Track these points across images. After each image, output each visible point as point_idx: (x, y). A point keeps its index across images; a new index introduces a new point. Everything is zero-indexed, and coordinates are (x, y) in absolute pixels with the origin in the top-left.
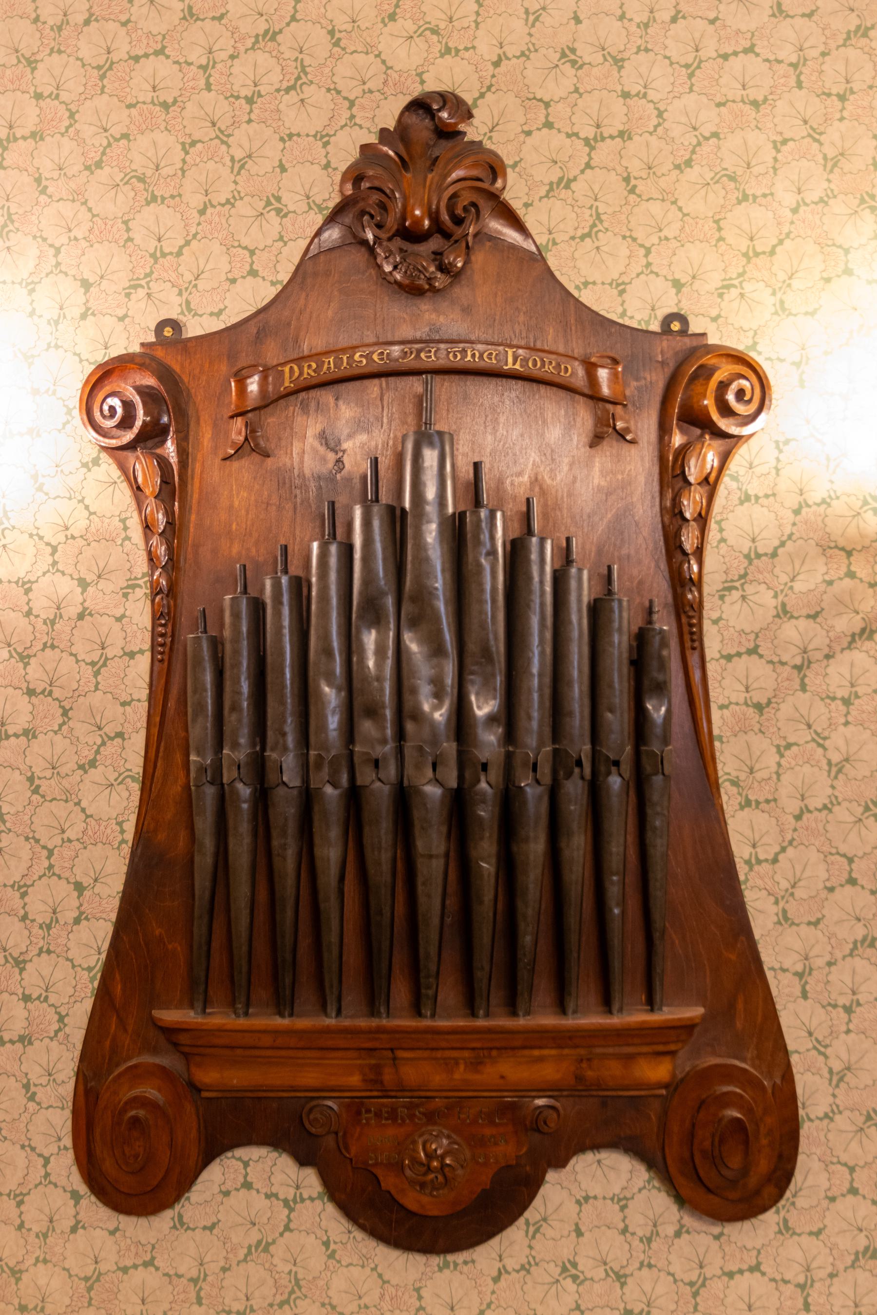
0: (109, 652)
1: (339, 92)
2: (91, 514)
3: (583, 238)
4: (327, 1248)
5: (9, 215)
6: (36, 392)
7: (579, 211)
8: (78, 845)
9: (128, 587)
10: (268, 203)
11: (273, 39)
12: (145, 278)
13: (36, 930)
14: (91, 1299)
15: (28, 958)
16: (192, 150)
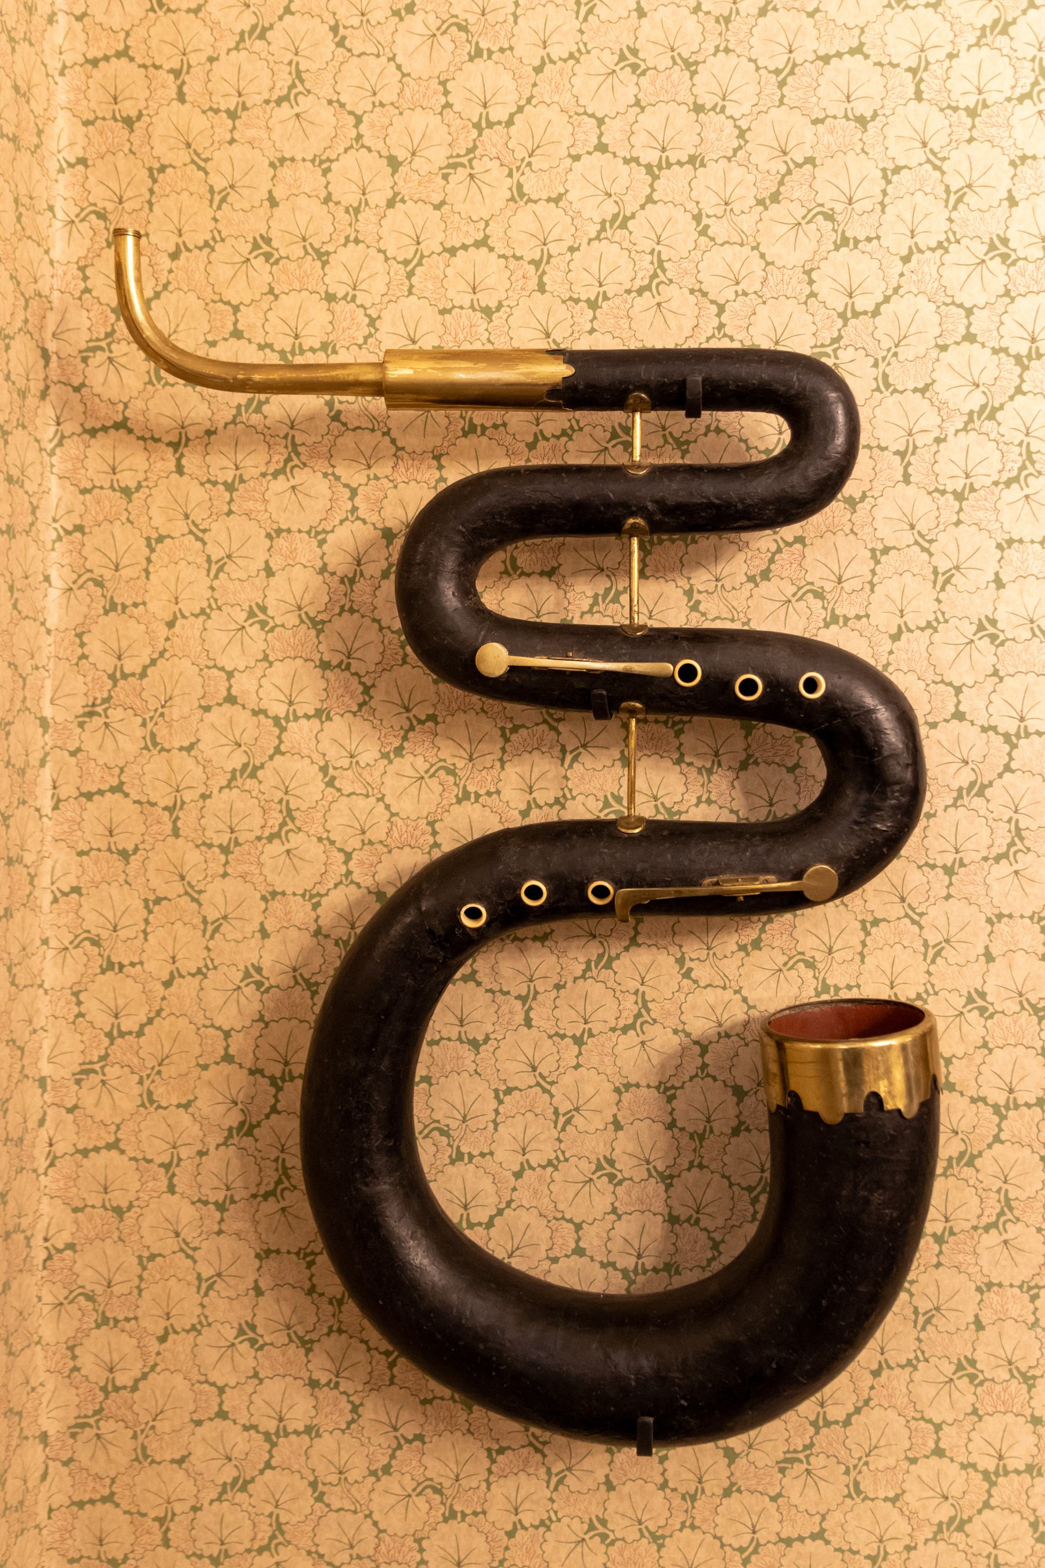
1: (705, 294)
3: (640, 291)
4: (682, 966)
5: (294, 445)
6: (325, 665)
7: (1005, 448)
9: (449, 166)
10: (592, 1527)
14: (411, 286)
15: (701, 58)
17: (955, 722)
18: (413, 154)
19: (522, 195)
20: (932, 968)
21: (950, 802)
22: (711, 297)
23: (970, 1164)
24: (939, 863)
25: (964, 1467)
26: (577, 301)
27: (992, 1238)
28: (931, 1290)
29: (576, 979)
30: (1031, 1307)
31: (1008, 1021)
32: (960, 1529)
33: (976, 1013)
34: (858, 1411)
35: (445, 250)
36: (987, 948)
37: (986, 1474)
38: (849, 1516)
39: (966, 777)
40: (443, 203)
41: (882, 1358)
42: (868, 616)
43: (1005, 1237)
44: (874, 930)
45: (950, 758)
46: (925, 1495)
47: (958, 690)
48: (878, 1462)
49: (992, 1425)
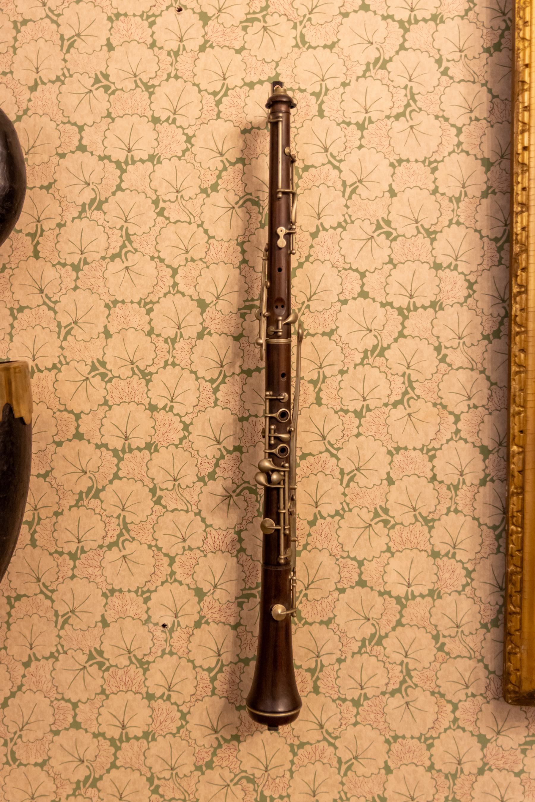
0: (230, 82)
2: (207, 526)
3: (397, 117)
4: (154, 495)
8: (198, 553)
9: (247, 20)
11: (383, 67)
12: (261, 11)
13: (161, 344)
16: (301, 752)
17: (79, 153)
18: (220, 11)
19: (304, 42)
20: (64, 344)
21: (76, 214)
22: (451, 121)
23: (96, 496)
24: (69, 262)
25: (95, 736)
26: (349, 124)
27: (114, 554)
28: (68, 597)
29: (354, 654)
30: (145, 607)
31: (123, 383)
32: (93, 785)
33: (98, 378)
34: (13, 695)
35: (245, 84)
36: (105, 327)
37: (112, 741)
38: (7, 779)
39: (87, 196)
40: (243, 48)
41: (31, 652)
42: (11, 72)
43: (124, 553)
44: (20, 315)
45: (76, 181)
46: (66, 760)
47: (81, 129)
48: (29, 735)
49: (116, 702)
